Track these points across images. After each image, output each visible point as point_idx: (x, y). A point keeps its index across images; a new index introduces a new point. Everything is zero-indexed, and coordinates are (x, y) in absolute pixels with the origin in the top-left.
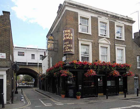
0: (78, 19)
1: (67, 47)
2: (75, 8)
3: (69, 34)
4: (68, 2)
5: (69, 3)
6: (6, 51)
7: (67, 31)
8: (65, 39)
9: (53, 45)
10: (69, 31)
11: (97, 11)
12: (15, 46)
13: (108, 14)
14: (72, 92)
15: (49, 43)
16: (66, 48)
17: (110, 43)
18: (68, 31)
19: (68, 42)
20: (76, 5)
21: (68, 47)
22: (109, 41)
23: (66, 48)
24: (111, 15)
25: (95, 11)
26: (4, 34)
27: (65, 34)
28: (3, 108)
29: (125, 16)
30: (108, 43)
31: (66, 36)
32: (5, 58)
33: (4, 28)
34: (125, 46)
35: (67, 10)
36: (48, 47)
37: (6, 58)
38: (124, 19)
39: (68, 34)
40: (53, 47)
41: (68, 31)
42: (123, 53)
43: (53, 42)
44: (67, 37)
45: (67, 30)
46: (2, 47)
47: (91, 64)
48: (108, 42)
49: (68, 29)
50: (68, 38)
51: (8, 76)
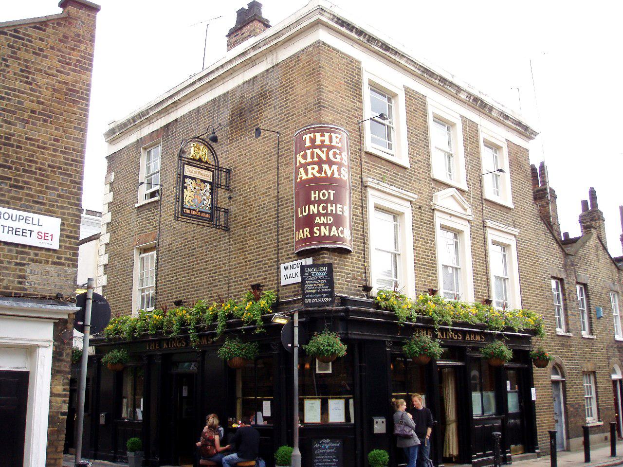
0: (359, 89)
1: (326, 215)
3: (335, 154)
6: (63, 208)
7: (327, 138)
8: (317, 175)
9: (208, 194)
13: (459, 89)
15: (190, 177)
16: (324, 220)
17: (469, 212)
18: (331, 141)
19: (332, 192)
22: (467, 205)
23: (324, 220)
24: (469, 95)
25: (419, 69)
26: (62, 114)
27: (317, 151)
30: (461, 210)
31: (320, 162)
32: (55, 245)
33: (62, 77)
34: (516, 231)
35: (324, 43)
36: (186, 201)
37: (60, 246)
38: (505, 119)
39: (331, 153)
40: (207, 203)
42: (22, 310)
43: (208, 176)
44: (326, 167)
46: (42, 181)
48: (465, 209)
49: (333, 132)
50: (333, 173)
51: (62, 355)
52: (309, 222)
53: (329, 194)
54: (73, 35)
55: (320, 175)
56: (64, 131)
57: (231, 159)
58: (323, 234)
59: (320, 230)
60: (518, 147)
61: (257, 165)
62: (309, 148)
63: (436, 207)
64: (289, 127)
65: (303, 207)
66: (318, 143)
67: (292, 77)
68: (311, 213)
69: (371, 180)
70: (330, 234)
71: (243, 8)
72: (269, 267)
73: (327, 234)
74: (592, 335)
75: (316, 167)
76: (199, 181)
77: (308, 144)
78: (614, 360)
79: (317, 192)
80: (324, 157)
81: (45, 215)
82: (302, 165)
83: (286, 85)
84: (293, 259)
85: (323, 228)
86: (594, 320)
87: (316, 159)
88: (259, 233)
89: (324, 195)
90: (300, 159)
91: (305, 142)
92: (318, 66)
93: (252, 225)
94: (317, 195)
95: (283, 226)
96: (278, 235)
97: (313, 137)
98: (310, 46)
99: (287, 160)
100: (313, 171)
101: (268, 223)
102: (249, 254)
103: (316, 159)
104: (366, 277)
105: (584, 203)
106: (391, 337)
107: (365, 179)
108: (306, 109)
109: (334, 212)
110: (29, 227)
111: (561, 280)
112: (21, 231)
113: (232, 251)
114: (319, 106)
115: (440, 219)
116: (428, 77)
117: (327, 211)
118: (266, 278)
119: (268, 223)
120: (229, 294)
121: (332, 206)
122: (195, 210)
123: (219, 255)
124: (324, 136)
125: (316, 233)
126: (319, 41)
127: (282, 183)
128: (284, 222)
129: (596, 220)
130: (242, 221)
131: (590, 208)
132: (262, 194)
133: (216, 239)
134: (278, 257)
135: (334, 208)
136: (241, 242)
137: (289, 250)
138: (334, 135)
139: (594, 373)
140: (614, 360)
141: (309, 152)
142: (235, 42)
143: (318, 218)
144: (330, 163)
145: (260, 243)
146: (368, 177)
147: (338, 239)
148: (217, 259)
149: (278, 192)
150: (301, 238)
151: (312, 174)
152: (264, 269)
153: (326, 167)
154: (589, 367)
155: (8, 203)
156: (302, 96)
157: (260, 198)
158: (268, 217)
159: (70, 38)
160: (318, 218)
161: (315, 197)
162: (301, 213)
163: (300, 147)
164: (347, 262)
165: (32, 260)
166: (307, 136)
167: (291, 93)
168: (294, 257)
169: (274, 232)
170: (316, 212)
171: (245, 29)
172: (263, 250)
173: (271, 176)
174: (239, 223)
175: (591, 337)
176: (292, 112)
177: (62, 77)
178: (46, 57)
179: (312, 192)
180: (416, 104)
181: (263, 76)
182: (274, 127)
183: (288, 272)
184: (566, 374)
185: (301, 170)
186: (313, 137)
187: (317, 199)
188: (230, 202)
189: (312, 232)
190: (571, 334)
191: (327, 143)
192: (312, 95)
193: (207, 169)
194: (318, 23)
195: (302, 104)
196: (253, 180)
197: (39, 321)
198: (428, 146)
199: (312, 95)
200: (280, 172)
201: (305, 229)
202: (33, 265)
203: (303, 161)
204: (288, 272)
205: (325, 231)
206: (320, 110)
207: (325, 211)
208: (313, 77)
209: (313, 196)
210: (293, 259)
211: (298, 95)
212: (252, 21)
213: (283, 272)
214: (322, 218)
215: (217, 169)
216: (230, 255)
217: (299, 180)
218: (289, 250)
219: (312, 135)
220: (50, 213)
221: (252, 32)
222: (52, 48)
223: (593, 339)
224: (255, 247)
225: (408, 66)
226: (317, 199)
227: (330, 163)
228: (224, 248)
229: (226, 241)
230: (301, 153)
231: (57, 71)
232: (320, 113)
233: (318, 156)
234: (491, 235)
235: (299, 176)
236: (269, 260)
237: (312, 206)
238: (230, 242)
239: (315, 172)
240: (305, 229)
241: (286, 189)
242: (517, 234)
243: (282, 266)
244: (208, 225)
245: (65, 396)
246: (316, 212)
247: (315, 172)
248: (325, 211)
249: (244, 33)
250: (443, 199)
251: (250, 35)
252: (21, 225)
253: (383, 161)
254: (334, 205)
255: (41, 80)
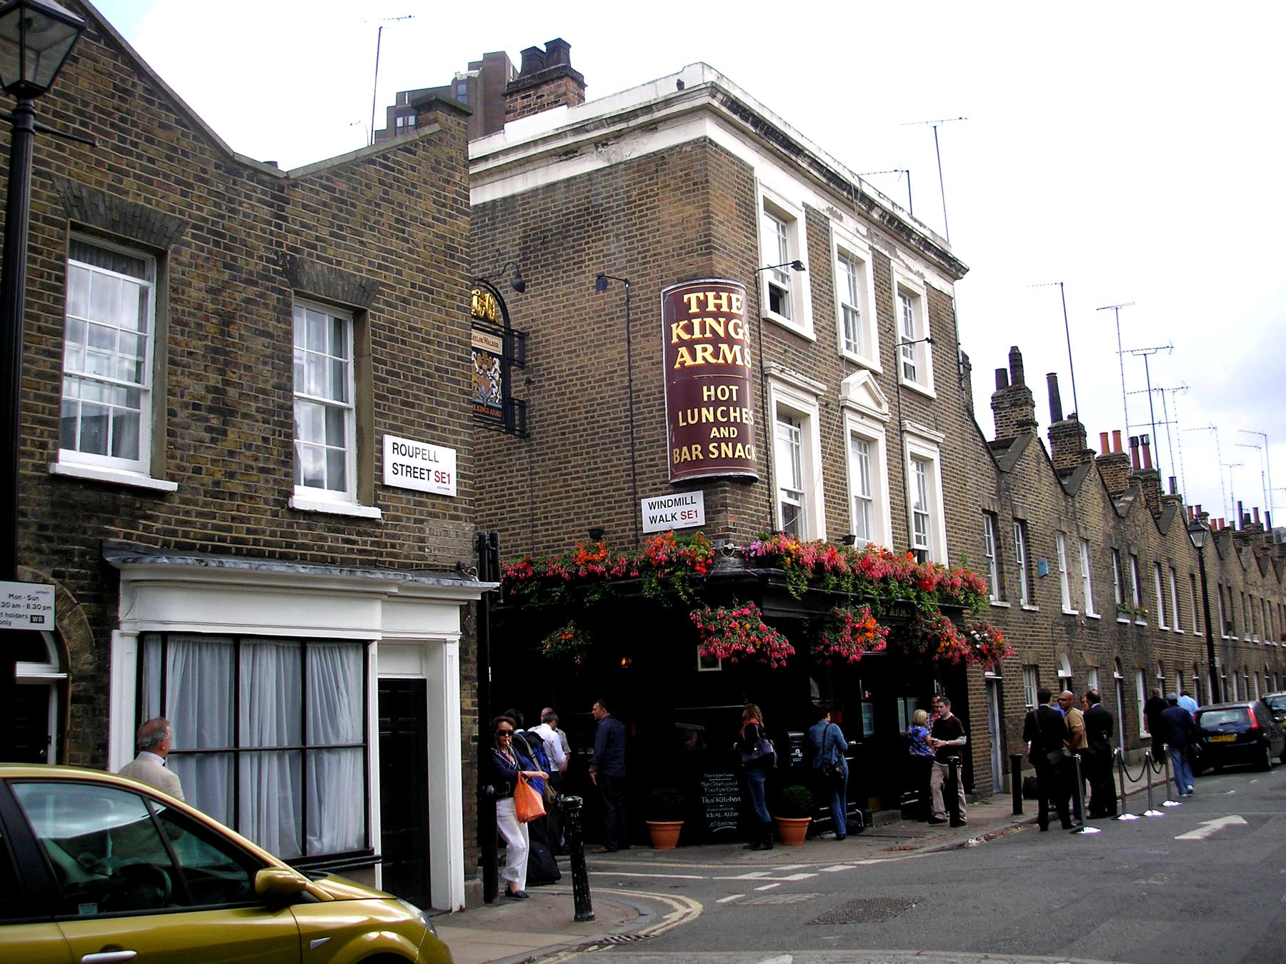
1: (728, 424)
2: (743, 131)
3: (736, 326)
4: (726, 94)
5: (729, 98)
7: (724, 302)
9: (497, 376)
10: (735, 304)
11: (834, 177)
12: (65, 370)
13: (871, 204)
14: (727, 795)
16: (724, 432)
17: (885, 408)
18: (730, 306)
20: (758, 121)
21: (735, 424)
22: (882, 397)
23: (724, 432)
25: (824, 176)
27: (709, 321)
28: (583, 920)
29: (925, 227)
30: (873, 405)
31: (716, 340)
32: (451, 489)
33: (441, 229)
34: (940, 436)
35: (711, 142)
41: (730, 300)
44: (724, 347)
45: (724, 295)
47: (879, 562)
48: (879, 404)
49: (731, 291)
50: (735, 359)
52: (698, 434)
53: (731, 391)
54: (445, 158)
55: (715, 361)
56: (447, 314)
57: (526, 316)
58: (723, 456)
59: (719, 448)
60: (939, 294)
61: (585, 332)
62: (696, 316)
63: (848, 404)
64: (648, 274)
65: (689, 411)
66: (711, 308)
67: (651, 190)
68: (704, 421)
69: (774, 365)
70: (734, 455)
71: (535, 48)
72: (615, 502)
73: (730, 455)
74: (1034, 604)
75: (710, 348)
76: (485, 355)
77: (694, 309)
78: (1061, 645)
79: (712, 387)
80: (721, 331)
81: (438, 445)
82: (682, 342)
83: (638, 203)
84: (664, 491)
85: (723, 445)
86: (1036, 582)
87: (708, 335)
88: (593, 446)
89: (723, 394)
90: (678, 331)
91: (689, 305)
92: (704, 180)
93: (578, 431)
94: (713, 392)
95: (643, 437)
96: (633, 451)
97: (702, 298)
98: (688, 143)
99: (647, 329)
100: (705, 354)
101: (610, 431)
102: (573, 479)
103: (708, 335)
104: (771, 519)
105: (1000, 374)
106: (808, 614)
107: (766, 363)
108: (681, 248)
109: (739, 420)
110: (426, 465)
111: (993, 515)
112: (418, 470)
113: (537, 473)
114: (707, 246)
115: (852, 423)
116: (834, 187)
117: (729, 419)
118: (613, 520)
119: (610, 431)
120: (533, 543)
121: (735, 411)
122: (482, 405)
123: (508, 477)
124: (720, 298)
125: (713, 454)
126: (705, 137)
127: (638, 367)
128: (645, 430)
129: (1021, 406)
130: (557, 423)
131: (1010, 384)
132: (596, 381)
133: (500, 451)
134: (634, 487)
135: (738, 414)
136: (557, 458)
137: (657, 477)
138: (734, 296)
139: (1035, 668)
140: (1061, 645)
141: (696, 322)
142: (524, 107)
143: (715, 429)
144: (731, 342)
145: (596, 463)
146: (770, 360)
147: (742, 462)
148: (505, 484)
149: (631, 381)
150: (686, 459)
151: (704, 358)
152: (607, 506)
153: (724, 347)
154: (1030, 658)
155: (401, 429)
156: (672, 226)
157: (593, 388)
158: (611, 419)
159: (443, 164)
160: (715, 429)
161: (709, 396)
162: (685, 419)
163: (679, 311)
164: (750, 497)
165: (430, 514)
166: (693, 297)
167: (649, 217)
168: (667, 489)
169: (625, 446)
170: (711, 419)
171: (545, 89)
172: (602, 474)
173: (616, 352)
174: (548, 425)
175: (1033, 608)
176: (654, 249)
177: (441, 229)
178: (419, 196)
179: (705, 388)
180: (818, 229)
181: (590, 180)
182: (617, 270)
183: (657, 512)
184: (1003, 670)
185: (683, 350)
186: (702, 298)
187: (713, 399)
188: (529, 390)
189: (705, 451)
190: (1008, 605)
191: (725, 309)
192: (693, 227)
193: (495, 333)
194: (707, 109)
195: (674, 238)
196: (578, 356)
197: (217, 590)
198: (833, 302)
199: (693, 227)
200: (633, 347)
201: (693, 447)
202: (432, 521)
203: (686, 337)
204: (657, 512)
205: (727, 450)
206: (710, 253)
207: (726, 419)
208: (695, 196)
209: (706, 393)
210: (664, 491)
211: (663, 223)
212: (560, 78)
213: (646, 512)
214: (722, 429)
215: (508, 335)
216: (532, 480)
217: (677, 366)
218: (657, 477)
219: (701, 295)
220: (442, 442)
221: (560, 96)
222: (425, 182)
223: (1034, 612)
224: (586, 468)
225: (812, 171)
226: (713, 399)
227: (731, 342)
228: (518, 467)
229: (524, 455)
230: (682, 323)
231: (433, 218)
232: (711, 259)
233: (713, 330)
234: (912, 446)
235: (679, 360)
236: (615, 490)
237: (704, 411)
238: (531, 457)
239: (708, 355)
240: (693, 447)
241: (645, 377)
242: (941, 441)
243: (645, 503)
244: (482, 425)
245: (474, 713)
246: (711, 419)
247: (708, 355)
248: (726, 419)
249: (543, 96)
250: (856, 389)
251: (556, 102)
252: (417, 462)
253: (784, 332)
254: (738, 409)
255: (420, 235)
